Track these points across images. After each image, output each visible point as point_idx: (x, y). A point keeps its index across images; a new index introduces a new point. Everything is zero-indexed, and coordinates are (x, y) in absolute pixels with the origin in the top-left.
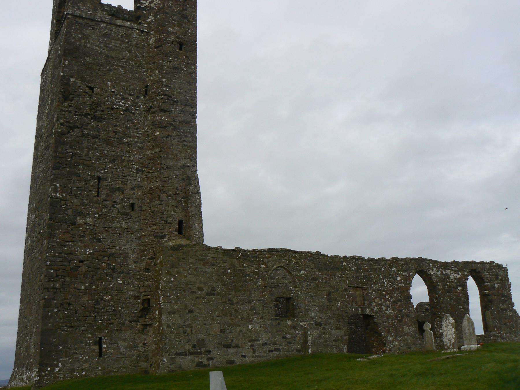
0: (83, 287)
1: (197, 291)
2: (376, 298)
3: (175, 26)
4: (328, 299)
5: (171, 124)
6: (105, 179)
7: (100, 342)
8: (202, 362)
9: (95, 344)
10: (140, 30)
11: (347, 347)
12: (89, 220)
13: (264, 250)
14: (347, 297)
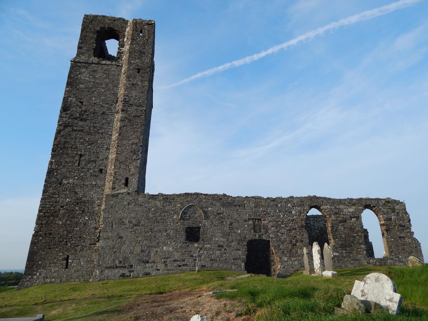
0: (61, 223)
1: (331, 245)
2: (272, 227)
3: (136, 59)
4: (230, 228)
5: (127, 118)
6: (85, 155)
7: (67, 259)
8: (125, 274)
9: (64, 259)
10: (117, 65)
11: (245, 264)
12: (71, 181)
13: (180, 195)
14: (246, 226)
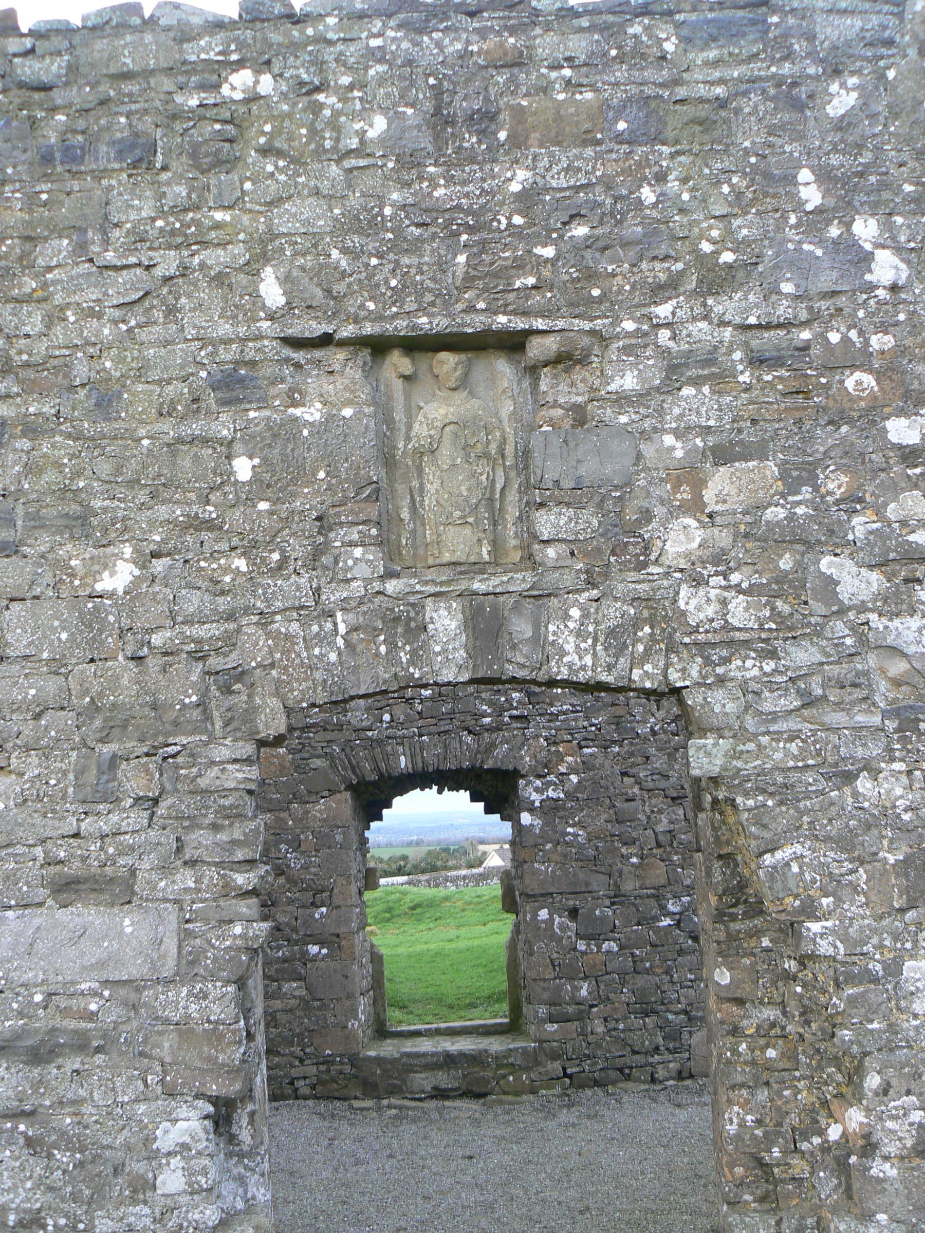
2: (723, 455)
14: (243, 468)
